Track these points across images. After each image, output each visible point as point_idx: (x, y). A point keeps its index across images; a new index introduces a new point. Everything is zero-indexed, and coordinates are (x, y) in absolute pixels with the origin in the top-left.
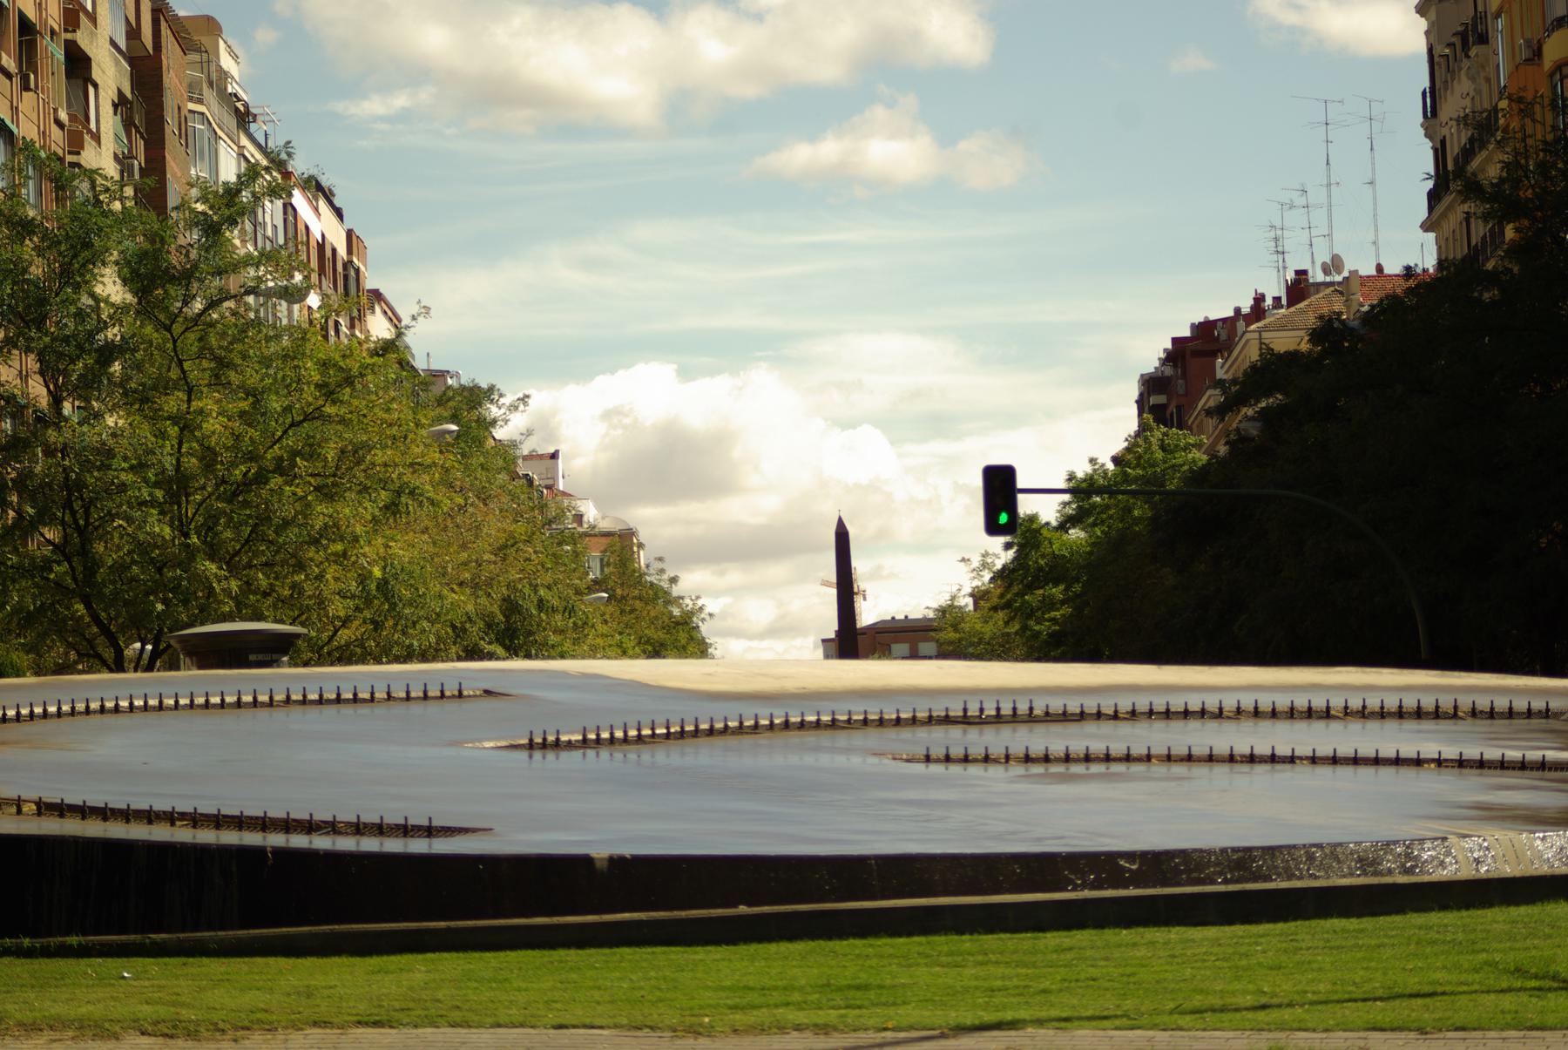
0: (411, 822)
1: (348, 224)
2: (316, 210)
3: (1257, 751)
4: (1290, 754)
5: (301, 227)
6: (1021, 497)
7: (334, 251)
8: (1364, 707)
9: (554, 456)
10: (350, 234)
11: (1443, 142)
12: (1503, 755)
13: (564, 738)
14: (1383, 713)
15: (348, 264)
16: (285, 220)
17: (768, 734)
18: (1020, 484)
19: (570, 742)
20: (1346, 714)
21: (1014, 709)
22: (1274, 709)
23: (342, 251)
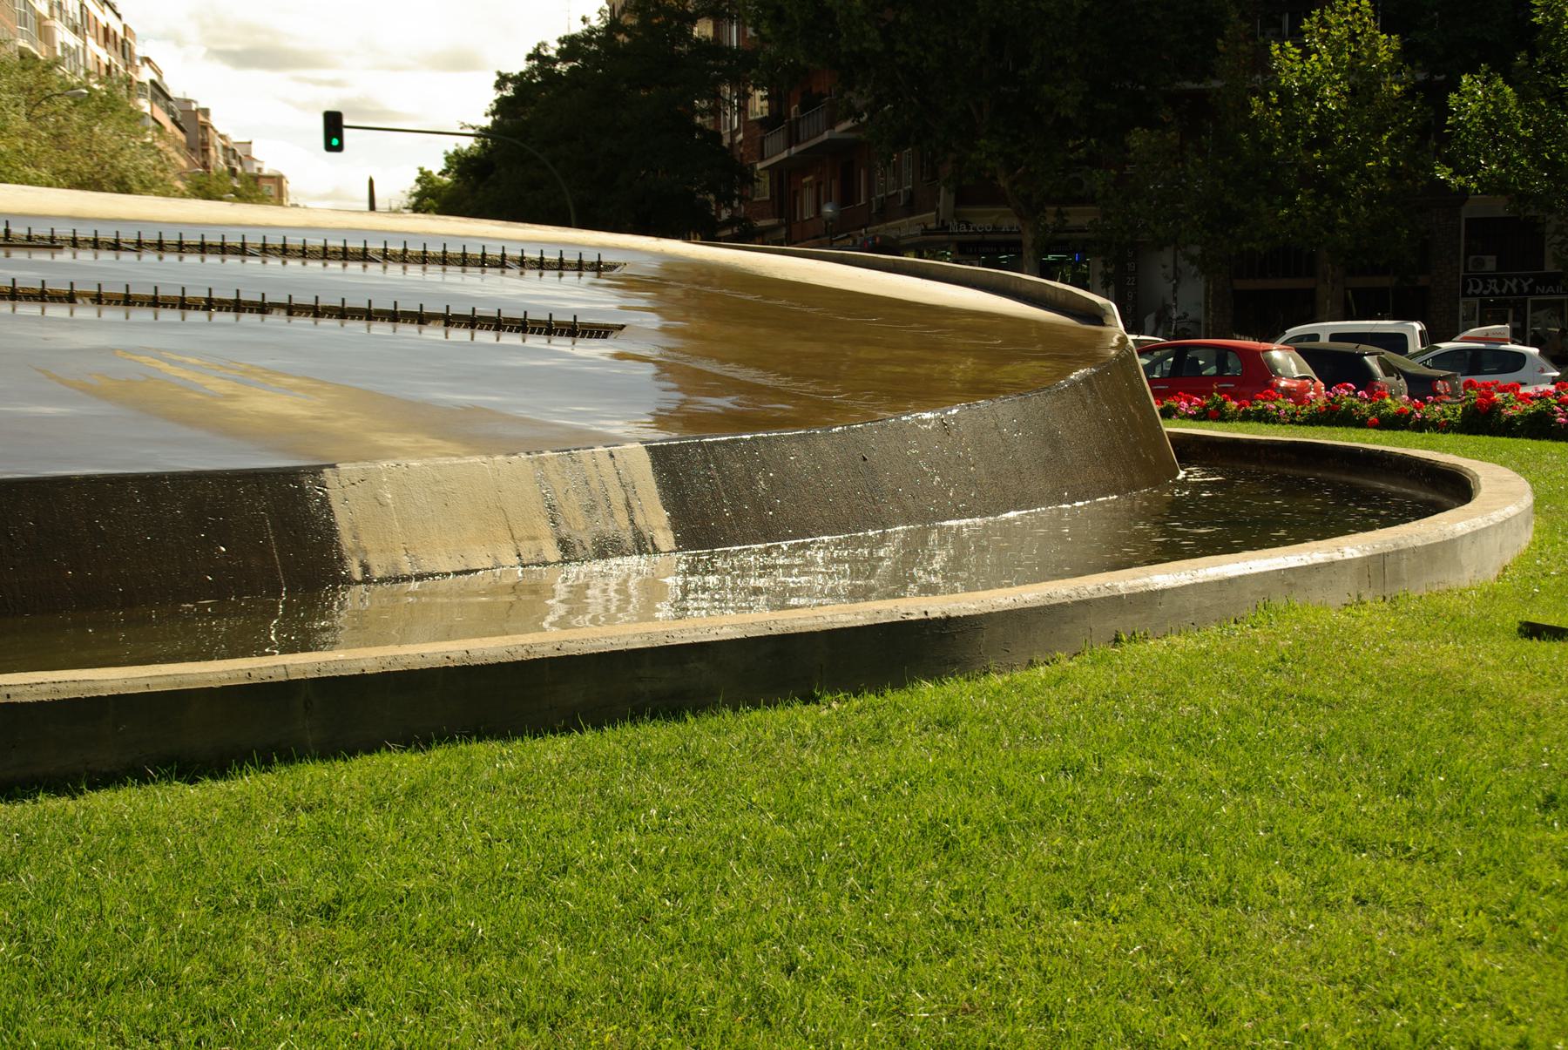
2: (103, 11)
5: (91, 17)
6: (346, 131)
7: (115, 33)
8: (405, 251)
9: (250, 143)
10: (125, 26)
11: (614, 6)
12: (524, 341)
14: (444, 257)
15: (123, 41)
16: (82, 13)
20: (483, 262)
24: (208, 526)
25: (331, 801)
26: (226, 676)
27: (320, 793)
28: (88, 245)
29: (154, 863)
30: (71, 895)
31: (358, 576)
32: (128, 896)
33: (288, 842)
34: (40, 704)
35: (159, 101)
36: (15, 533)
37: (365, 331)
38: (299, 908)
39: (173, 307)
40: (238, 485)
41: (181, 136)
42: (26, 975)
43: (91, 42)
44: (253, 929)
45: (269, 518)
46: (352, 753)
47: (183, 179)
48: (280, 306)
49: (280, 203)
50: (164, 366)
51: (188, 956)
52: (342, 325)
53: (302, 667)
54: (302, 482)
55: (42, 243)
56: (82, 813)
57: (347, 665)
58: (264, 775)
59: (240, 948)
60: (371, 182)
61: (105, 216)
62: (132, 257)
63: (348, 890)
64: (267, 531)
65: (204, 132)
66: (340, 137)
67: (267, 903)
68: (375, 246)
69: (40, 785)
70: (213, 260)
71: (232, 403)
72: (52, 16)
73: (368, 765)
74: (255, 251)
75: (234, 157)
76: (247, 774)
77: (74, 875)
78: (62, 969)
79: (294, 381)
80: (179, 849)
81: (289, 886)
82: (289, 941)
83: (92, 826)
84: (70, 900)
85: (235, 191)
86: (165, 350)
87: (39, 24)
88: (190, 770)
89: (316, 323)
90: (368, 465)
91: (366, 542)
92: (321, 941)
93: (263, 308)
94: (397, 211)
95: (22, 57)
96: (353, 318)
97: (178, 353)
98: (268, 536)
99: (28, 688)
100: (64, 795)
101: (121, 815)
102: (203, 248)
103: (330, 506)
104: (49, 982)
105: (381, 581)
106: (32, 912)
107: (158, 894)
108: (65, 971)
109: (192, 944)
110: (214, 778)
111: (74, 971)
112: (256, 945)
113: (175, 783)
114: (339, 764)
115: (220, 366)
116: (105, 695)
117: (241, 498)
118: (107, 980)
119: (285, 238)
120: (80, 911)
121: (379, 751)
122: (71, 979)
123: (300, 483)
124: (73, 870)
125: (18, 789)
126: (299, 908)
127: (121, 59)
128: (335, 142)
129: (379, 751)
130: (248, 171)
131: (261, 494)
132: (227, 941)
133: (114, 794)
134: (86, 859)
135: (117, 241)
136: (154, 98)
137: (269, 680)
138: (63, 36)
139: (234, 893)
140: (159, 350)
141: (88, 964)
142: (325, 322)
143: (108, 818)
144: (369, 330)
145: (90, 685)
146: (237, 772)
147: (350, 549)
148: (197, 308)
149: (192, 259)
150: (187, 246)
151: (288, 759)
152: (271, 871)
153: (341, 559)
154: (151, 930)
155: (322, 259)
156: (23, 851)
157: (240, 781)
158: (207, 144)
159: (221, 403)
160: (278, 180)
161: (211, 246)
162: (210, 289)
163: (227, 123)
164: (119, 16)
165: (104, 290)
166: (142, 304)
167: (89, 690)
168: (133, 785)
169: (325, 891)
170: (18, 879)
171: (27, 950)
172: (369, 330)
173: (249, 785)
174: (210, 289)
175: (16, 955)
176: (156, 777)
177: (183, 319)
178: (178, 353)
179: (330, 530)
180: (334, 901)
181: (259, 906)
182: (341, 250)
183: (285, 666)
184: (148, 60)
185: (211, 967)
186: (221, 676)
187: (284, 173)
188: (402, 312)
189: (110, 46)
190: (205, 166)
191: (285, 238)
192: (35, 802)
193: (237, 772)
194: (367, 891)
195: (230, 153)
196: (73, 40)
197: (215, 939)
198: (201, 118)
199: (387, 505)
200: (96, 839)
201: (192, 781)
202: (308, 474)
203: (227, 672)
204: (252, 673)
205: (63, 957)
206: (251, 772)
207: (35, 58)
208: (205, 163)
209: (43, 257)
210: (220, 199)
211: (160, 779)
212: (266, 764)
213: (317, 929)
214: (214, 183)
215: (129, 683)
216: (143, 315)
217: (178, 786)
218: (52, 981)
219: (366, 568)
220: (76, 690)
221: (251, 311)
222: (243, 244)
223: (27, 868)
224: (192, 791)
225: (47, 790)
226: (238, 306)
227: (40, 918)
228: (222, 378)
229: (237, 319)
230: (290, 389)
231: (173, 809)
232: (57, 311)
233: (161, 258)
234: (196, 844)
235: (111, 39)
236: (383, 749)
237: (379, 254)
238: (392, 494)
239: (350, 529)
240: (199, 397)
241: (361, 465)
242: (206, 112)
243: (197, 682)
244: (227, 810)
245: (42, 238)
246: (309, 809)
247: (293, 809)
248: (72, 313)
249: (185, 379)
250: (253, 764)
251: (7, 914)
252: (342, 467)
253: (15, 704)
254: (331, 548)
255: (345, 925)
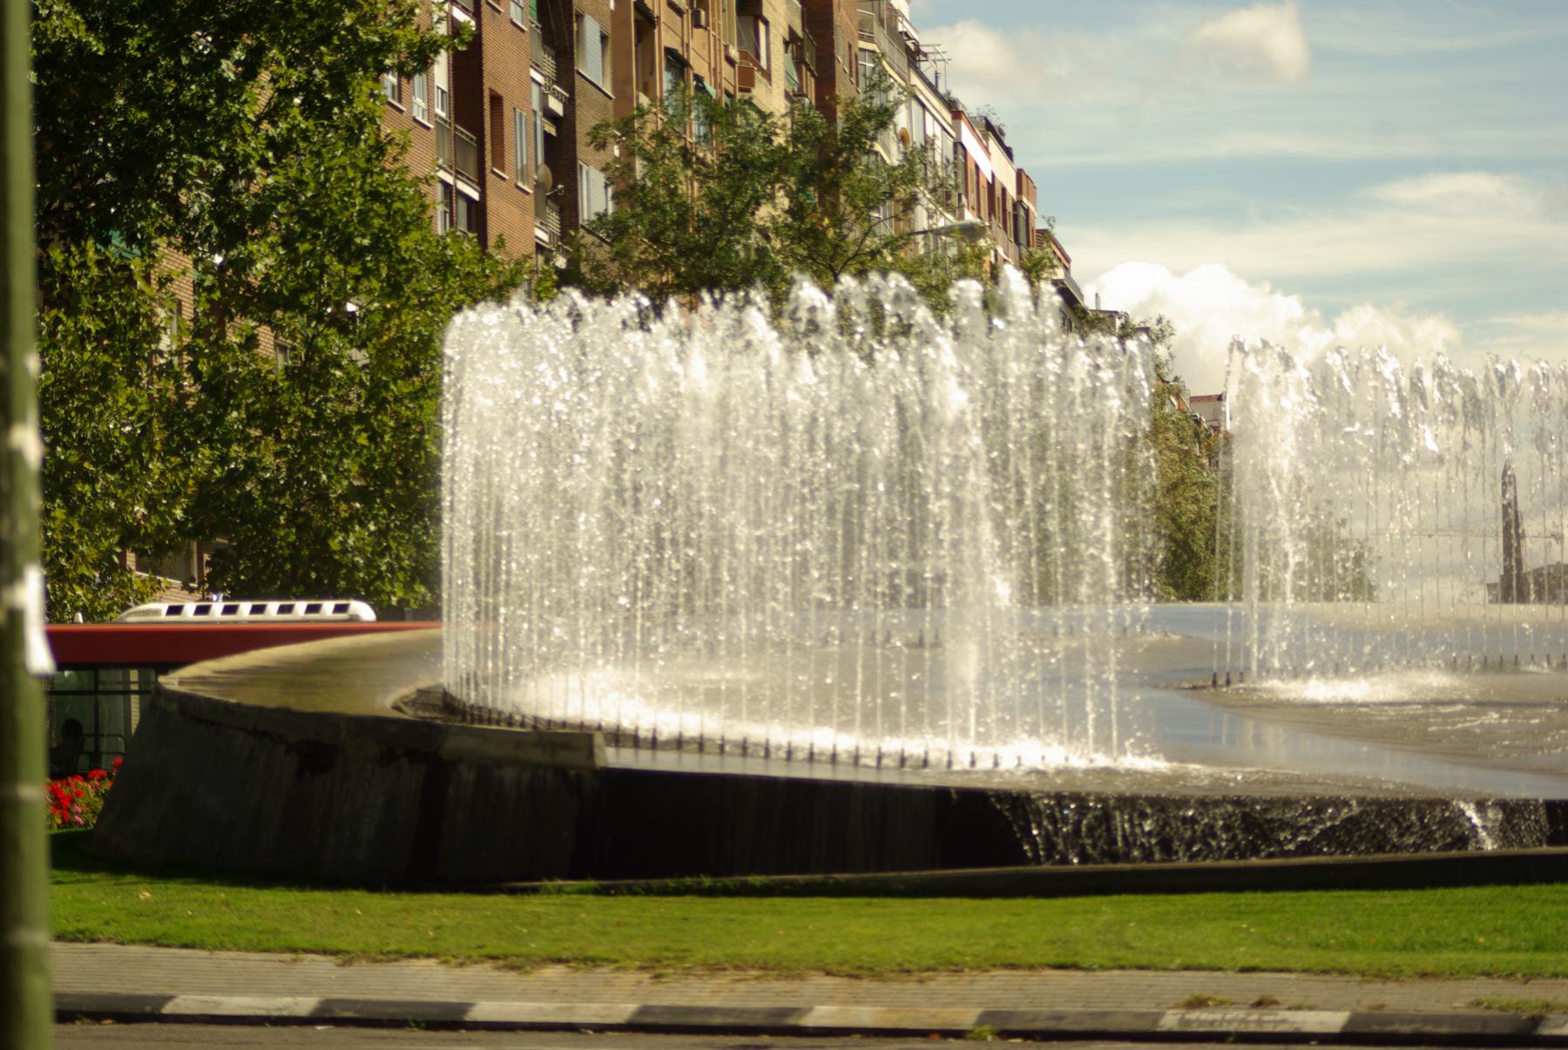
2: (986, 149)
5: (971, 167)
7: (1004, 190)
9: (1220, 398)
15: (1018, 204)
23: (1012, 191)
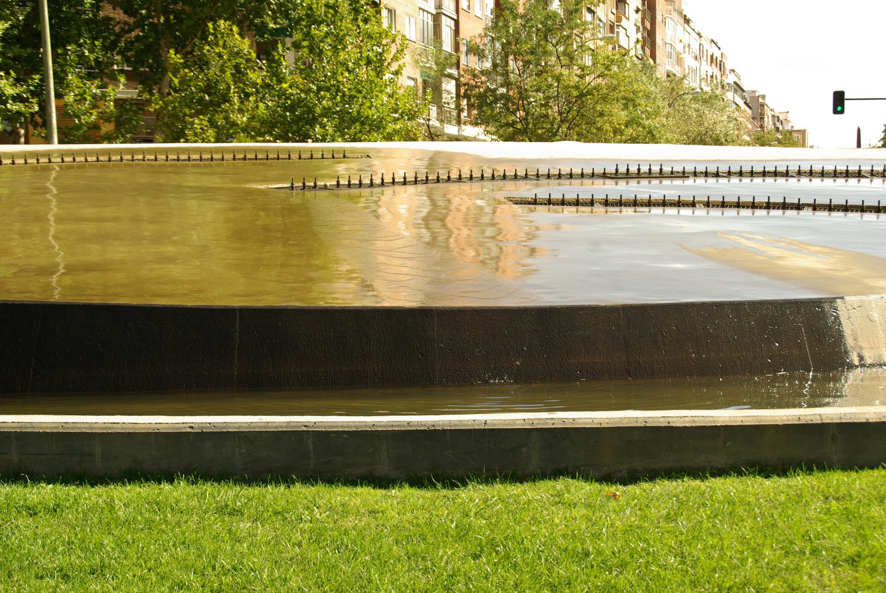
0: (834, 203)
1: (722, 51)
3: (639, 197)
4: (782, 201)
6: (846, 102)
10: (722, 53)
13: (320, 183)
16: (700, 49)
17: (513, 183)
18: (846, 97)
19: (326, 186)
21: (639, 170)
22: (811, 170)
24: (768, 331)
25: (850, 496)
26: (786, 418)
27: (843, 490)
28: (702, 175)
29: (749, 523)
30: (706, 535)
31: (856, 362)
32: (736, 539)
33: (826, 518)
34: (685, 428)
35: (738, 93)
36: (666, 333)
37: (860, 219)
38: (835, 558)
39: (748, 207)
40: (786, 309)
41: (749, 111)
42: (684, 577)
43: (704, 63)
44: (808, 567)
45: (804, 327)
46: (862, 468)
47: (750, 136)
48: (808, 205)
49: (804, 145)
50: (743, 241)
51: (772, 578)
52: (846, 216)
53: (830, 416)
54: (823, 307)
55: (678, 175)
56: (708, 490)
57: (858, 416)
58: (808, 477)
59: (802, 578)
60: (859, 131)
61: (700, 159)
62: (725, 180)
63: (864, 550)
64: (803, 335)
65: (762, 108)
66: (843, 106)
67: (815, 552)
68: (866, 168)
69: (685, 472)
70: (769, 180)
71: (783, 262)
72: (684, 52)
73: (871, 476)
74: (794, 174)
75: (778, 121)
76: (798, 475)
77: (706, 524)
78: (703, 576)
79: (817, 248)
80: (762, 515)
81: (828, 544)
82: (830, 576)
83: (714, 498)
84: (705, 537)
85: (778, 140)
86: (745, 232)
87: (678, 57)
88: (765, 470)
89: (830, 215)
90: (864, 298)
91: (861, 343)
92: (849, 579)
93: (799, 207)
94: (879, 147)
95: (668, 76)
96: (852, 211)
97: (751, 233)
98: (803, 338)
99: (679, 419)
100: (698, 479)
101: (729, 493)
102: (764, 174)
103: (840, 321)
104: (696, 582)
105: (872, 366)
106: (686, 542)
107: (753, 540)
108: (705, 577)
109: (773, 571)
110: (779, 476)
111: (710, 578)
112: (810, 576)
113: (757, 477)
114: (854, 474)
115: (774, 240)
116: (719, 425)
117: (787, 316)
118: (728, 585)
119: (811, 166)
120: (711, 545)
121: (878, 468)
122: (708, 582)
123: (822, 308)
124: (705, 521)
125: (674, 474)
126: (835, 558)
127: (719, 72)
128: (839, 108)
129: (878, 468)
130: (786, 128)
131: (799, 313)
132: (793, 572)
133: (724, 480)
134: (712, 516)
135: (718, 172)
136: (735, 91)
137: (811, 422)
138: (689, 61)
139: (796, 544)
140: (741, 232)
141: (717, 575)
142: (835, 214)
143: (722, 494)
144: (862, 217)
145: (711, 419)
146: (793, 474)
147: (852, 347)
148: (761, 208)
149: (758, 180)
150: (755, 173)
151: (822, 468)
152: (817, 533)
153: (846, 352)
154: (750, 560)
155: (833, 177)
156: (679, 508)
157: (794, 479)
158: (764, 114)
159: (776, 262)
160: (803, 132)
161: (768, 172)
162: (769, 197)
163: (775, 104)
164: (719, 48)
165: (787, 201)
166: (731, 207)
167: (711, 422)
168: (734, 476)
169: (850, 549)
170: (677, 523)
171: (685, 563)
172: (862, 217)
173: (800, 481)
174: (769, 197)
175: (679, 565)
176: (747, 473)
177: (753, 214)
178: (751, 233)
179: (840, 336)
180: (856, 556)
181: (811, 554)
182: (844, 171)
183: (820, 415)
184: (733, 71)
185: (785, 585)
186: (783, 418)
187: (806, 128)
188: (850, 205)
189: (714, 65)
190: (762, 127)
191: (811, 166)
192: (683, 481)
193: (793, 474)
194: (876, 552)
195: (776, 119)
196: (695, 64)
197: (786, 570)
198: (761, 100)
199: (875, 321)
200: (717, 505)
201: (767, 477)
202: (827, 302)
203: (787, 416)
204: (801, 417)
205: (703, 569)
206: (800, 474)
207: (675, 75)
208: (762, 125)
209: (678, 182)
210: (770, 145)
211: (749, 474)
212: (810, 470)
213: (847, 572)
214: (766, 136)
215: (732, 419)
216: (731, 212)
217: (759, 479)
218: (699, 582)
219: (861, 358)
220: (703, 422)
221: (792, 209)
222: (787, 171)
223: (682, 517)
224: (767, 482)
225: (689, 475)
226: (784, 206)
227: (690, 545)
228: (776, 247)
229: (784, 213)
230: (815, 253)
231: (757, 492)
232: (686, 212)
233: (741, 181)
234: (772, 514)
235: (714, 61)
236: (880, 467)
237: (868, 173)
238: (878, 314)
239: (852, 335)
240: (762, 258)
241: (859, 297)
242: (763, 97)
243: (770, 421)
244: (788, 495)
245: (678, 172)
246: (837, 499)
247: (827, 498)
248: (693, 213)
249: (755, 248)
250: (802, 470)
251: (673, 542)
252: (847, 298)
253: (672, 427)
254: (840, 346)
255: (863, 571)
